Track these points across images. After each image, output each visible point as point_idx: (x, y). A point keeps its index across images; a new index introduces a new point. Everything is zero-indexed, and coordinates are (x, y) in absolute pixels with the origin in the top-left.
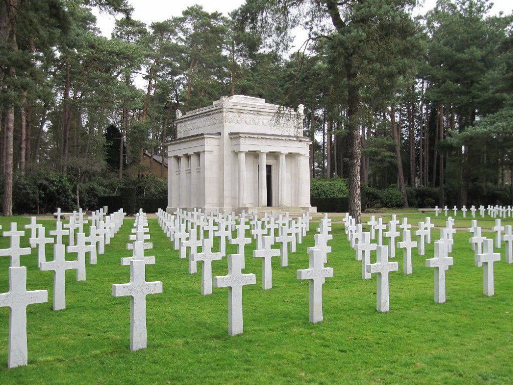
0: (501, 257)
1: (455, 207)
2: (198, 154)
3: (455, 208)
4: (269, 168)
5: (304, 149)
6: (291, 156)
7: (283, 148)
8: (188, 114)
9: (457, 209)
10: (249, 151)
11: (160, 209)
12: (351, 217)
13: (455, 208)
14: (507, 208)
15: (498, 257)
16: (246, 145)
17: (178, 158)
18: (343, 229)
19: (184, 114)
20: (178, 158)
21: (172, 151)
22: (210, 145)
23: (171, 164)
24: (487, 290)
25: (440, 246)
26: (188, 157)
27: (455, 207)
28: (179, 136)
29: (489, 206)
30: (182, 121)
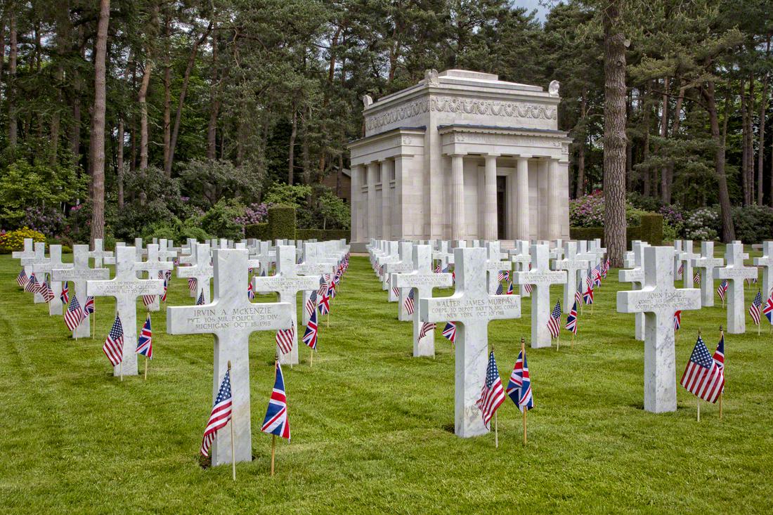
2: (392, 161)
4: (502, 181)
5: (559, 152)
6: (538, 164)
7: (525, 150)
10: (502, 156)
16: (463, 146)
20: (364, 168)
21: (359, 157)
22: (409, 145)
23: (355, 174)
26: (378, 165)
28: (367, 135)
30: (374, 112)
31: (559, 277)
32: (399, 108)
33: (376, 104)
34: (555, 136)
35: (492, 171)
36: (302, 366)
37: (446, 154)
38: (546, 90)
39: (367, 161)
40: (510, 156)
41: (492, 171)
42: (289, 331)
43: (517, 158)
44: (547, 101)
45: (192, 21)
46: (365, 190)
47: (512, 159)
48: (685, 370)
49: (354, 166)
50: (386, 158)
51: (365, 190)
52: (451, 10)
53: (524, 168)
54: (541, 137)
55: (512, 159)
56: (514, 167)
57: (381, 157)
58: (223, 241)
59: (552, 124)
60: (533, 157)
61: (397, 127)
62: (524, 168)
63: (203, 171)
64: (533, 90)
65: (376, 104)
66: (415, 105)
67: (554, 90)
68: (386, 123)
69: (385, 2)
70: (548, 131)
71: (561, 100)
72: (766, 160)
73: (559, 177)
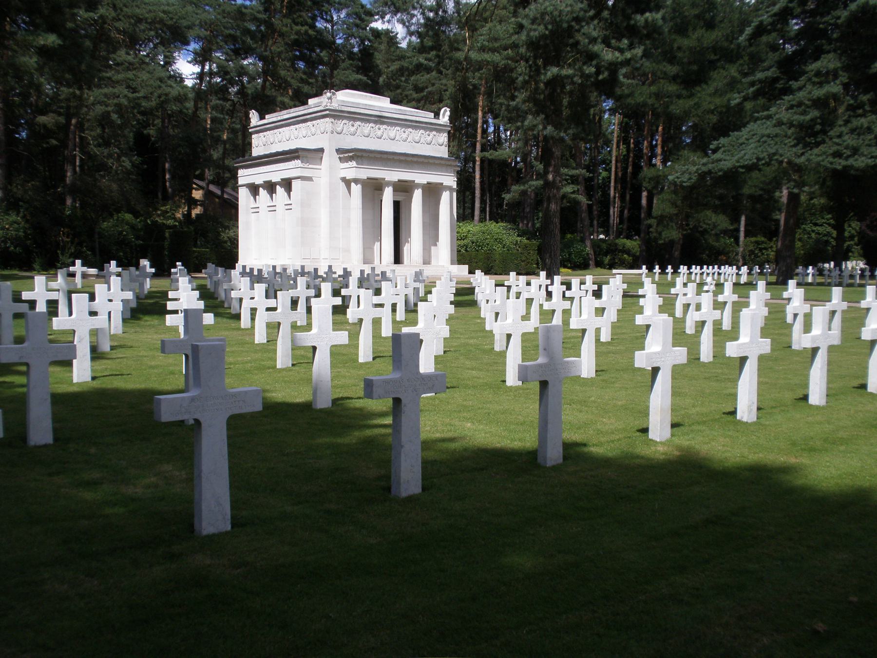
0: (724, 348)
1: (670, 267)
3: (657, 269)
4: (397, 205)
5: (450, 180)
8: (270, 118)
9: (672, 271)
10: (399, 181)
11: (644, 267)
12: (203, 271)
13: (657, 269)
14: (701, 268)
15: (680, 355)
17: (254, 189)
18: (471, 291)
19: (262, 117)
20: (254, 189)
21: (245, 176)
23: (244, 195)
24: (201, 524)
25: (403, 341)
27: (670, 267)
28: (256, 152)
29: (694, 267)
31: (407, 291)
34: (450, 163)
35: (388, 197)
36: (95, 382)
38: (437, 115)
39: (259, 180)
41: (388, 197)
42: (566, 338)
44: (438, 128)
45: (684, 52)
47: (406, 184)
48: (107, 378)
53: (418, 195)
54: (434, 164)
55: (406, 184)
56: (407, 192)
57: (276, 178)
58: (727, 266)
59: (443, 152)
61: (293, 147)
62: (418, 195)
64: (427, 116)
67: (445, 116)
68: (292, 137)
69: (418, 3)
73: (447, 205)
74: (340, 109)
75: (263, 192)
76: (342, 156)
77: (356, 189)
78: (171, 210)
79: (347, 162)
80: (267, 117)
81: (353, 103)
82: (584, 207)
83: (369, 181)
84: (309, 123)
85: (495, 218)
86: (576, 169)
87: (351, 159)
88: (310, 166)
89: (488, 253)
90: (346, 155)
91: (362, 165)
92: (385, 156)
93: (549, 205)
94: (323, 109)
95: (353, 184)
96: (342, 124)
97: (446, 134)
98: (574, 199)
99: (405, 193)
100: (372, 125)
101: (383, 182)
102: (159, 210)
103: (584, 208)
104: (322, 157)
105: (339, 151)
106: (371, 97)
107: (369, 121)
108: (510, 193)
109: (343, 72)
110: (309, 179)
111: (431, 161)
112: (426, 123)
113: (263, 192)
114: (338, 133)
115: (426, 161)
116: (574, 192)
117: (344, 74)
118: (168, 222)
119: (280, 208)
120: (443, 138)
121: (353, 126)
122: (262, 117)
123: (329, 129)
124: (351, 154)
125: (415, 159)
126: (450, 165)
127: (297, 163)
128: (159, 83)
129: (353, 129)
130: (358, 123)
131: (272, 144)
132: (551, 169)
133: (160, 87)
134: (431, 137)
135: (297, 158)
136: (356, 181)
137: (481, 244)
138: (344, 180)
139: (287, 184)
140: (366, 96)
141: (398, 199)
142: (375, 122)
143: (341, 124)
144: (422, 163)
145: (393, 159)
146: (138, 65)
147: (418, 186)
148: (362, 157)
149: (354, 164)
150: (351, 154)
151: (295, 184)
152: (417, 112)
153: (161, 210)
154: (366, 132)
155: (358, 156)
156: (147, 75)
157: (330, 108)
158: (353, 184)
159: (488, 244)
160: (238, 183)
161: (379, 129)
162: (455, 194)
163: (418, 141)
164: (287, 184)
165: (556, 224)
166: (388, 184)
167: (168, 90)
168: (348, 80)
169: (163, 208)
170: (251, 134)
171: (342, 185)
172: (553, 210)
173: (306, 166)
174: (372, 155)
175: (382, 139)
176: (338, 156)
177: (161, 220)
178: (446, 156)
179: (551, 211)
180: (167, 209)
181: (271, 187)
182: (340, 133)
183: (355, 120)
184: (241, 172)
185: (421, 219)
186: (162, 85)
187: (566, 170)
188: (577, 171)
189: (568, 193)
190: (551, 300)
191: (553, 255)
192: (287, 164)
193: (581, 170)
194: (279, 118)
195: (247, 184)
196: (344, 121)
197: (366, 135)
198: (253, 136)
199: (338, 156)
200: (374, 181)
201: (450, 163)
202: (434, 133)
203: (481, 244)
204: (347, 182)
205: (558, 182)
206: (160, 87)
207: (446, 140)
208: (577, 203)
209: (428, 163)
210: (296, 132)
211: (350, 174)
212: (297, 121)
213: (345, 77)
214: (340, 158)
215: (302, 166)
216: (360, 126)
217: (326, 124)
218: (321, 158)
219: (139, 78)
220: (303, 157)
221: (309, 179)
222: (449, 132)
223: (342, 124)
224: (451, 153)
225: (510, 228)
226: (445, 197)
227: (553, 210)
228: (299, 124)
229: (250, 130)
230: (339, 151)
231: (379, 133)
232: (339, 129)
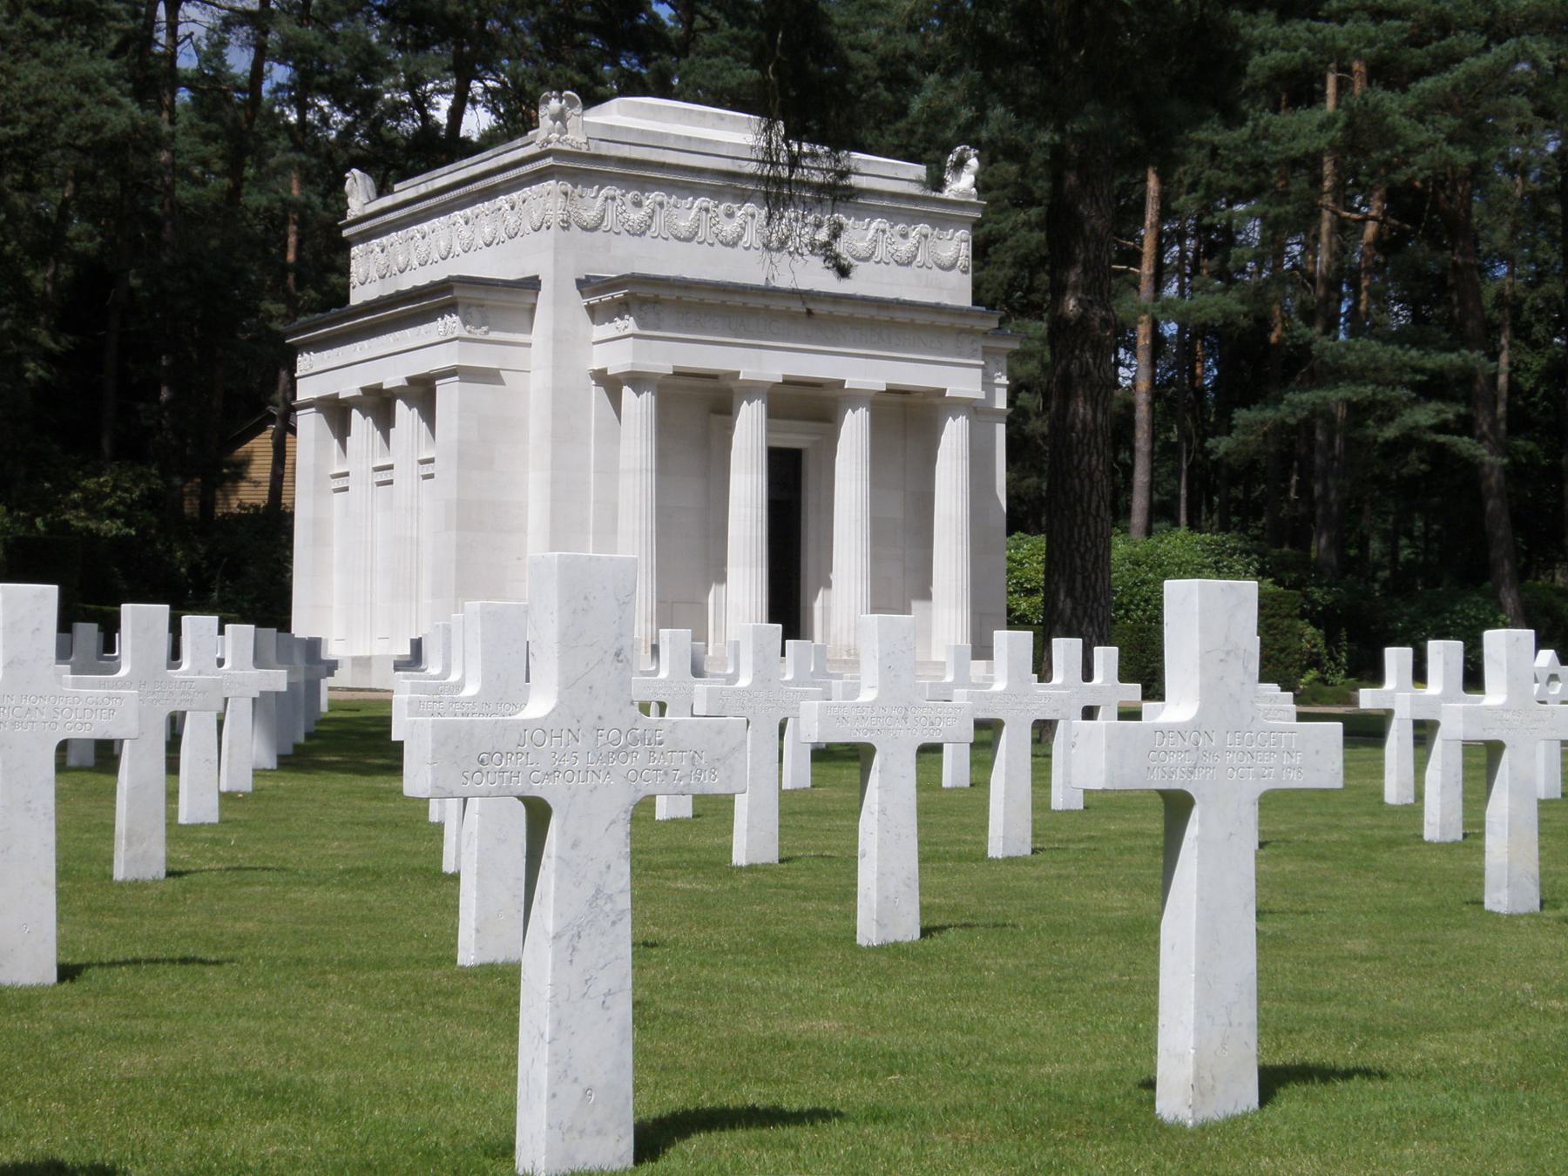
19: (383, 189)
20: (337, 412)
28: (357, 297)
32: (457, 215)
33: (387, 201)
34: (967, 323)
37: (604, 371)
39: (348, 386)
40: (712, 376)
43: (937, 401)
46: (384, 476)
49: (307, 405)
50: (409, 379)
51: (384, 476)
52: (254, 199)
53: (854, 429)
55: (825, 393)
57: (392, 376)
59: (956, 290)
60: (888, 391)
61: (438, 273)
62: (854, 429)
63: (1551, 15)
65: (387, 201)
66: (507, 206)
68: (458, 249)
70: (938, 309)
71: (984, 210)
72: (283, 374)
74: (592, 151)
75: (360, 423)
76: (594, 300)
77: (638, 406)
78: (115, 488)
79: (611, 321)
80: (397, 187)
81: (642, 133)
82: (1494, 480)
83: (681, 381)
84: (502, 201)
85: (1227, 530)
86: (1452, 350)
87: (620, 309)
88: (494, 335)
89: (1142, 630)
90: (606, 297)
91: (658, 328)
92: (737, 300)
93: (1066, 408)
94: (539, 150)
95: (627, 391)
96: (601, 199)
97: (964, 234)
98: (1442, 447)
99: (813, 424)
100: (702, 201)
101: (733, 385)
102: (75, 486)
103: (1493, 481)
104: (534, 305)
105: (587, 285)
106: (721, 117)
107: (694, 190)
108: (1229, 434)
109: (706, 62)
110: (490, 376)
111: (900, 316)
112: (894, 196)
113: (360, 423)
114: (584, 229)
115: (884, 315)
116: (1442, 428)
117: (709, 67)
118: (103, 527)
119: (406, 474)
120: (956, 245)
121: (638, 204)
122: (383, 189)
123: (555, 217)
124: (619, 294)
125: (843, 311)
126: (971, 332)
127: (450, 324)
128: (76, 94)
129: (636, 216)
130: (656, 196)
131: (401, 272)
132: (1073, 276)
133: (78, 106)
134: (912, 241)
135: (450, 308)
136: (637, 380)
137: (1125, 600)
138: (601, 377)
139: (422, 392)
140: (704, 114)
141: (790, 439)
142: (716, 194)
143: (593, 202)
144: (872, 324)
145: (767, 308)
146: (18, 43)
147: (856, 398)
148: (656, 301)
149: (629, 324)
150: (619, 294)
151: (447, 392)
152: (869, 162)
153: (83, 490)
154: (684, 224)
155: (643, 302)
156: (44, 70)
157: (560, 147)
158: (627, 391)
159: (1147, 601)
160: (294, 397)
161: (730, 215)
162: (1001, 431)
163: (864, 254)
164: (422, 392)
165: (1090, 476)
166: (752, 390)
167: (102, 112)
168: (720, 84)
169: (90, 484)
170: (346, 245)
171: (597, 395)
172: (1079, 426)
173: (479, 333)
174: (694, 296)
175: (740, 248)
176: (584, 302)
177: (82, 519)
178: (966, 301)
179: (1072, 428)
180: (101, 485)
181: (380, 404)
182: (594, 229)
183: (645, 185)
184: (305, 362)
185: (866, 507)
186: (86, 99)
187: (1414, 353)
188: (1454, 356)
189: (1416, 427)
190: (179, 666)
191: (1078, 585)
192: (423, 328)
193: (1465, 352)
194: (423, 189)
195: (321, 399)
196: (608, 191)
197: (685, 234)
198: (355, 251)
199: (584, 302)
200: (709, 384)
201: (967, 323)
202: (923, 228)
203: (1125, 600)
204: (611, 385)
205: (1097, 322)
206: (78, 106)
207: (966, 250)
208: (1471, 468)
209: (893, 324)
210: (465, 232)
211: (618, 359)
212: (469, 194)
213: (712, 77)
214: (591, 309)
215: (465, 334)
216: (661, 205)
217: (546, 198)
218: (532, 310)
219: (18, 79)
220: (469, 306)
221: (490, 376)
222: (976, 225)
223: (601, 199)
224: (979, 292)
225: (1235, 549)
226: (954, 435)
227: (1079, 426)
228: (473, 203)
229: (345, 233)
230: (587, 285)
231: (729, 228)
232: (589, 216)
